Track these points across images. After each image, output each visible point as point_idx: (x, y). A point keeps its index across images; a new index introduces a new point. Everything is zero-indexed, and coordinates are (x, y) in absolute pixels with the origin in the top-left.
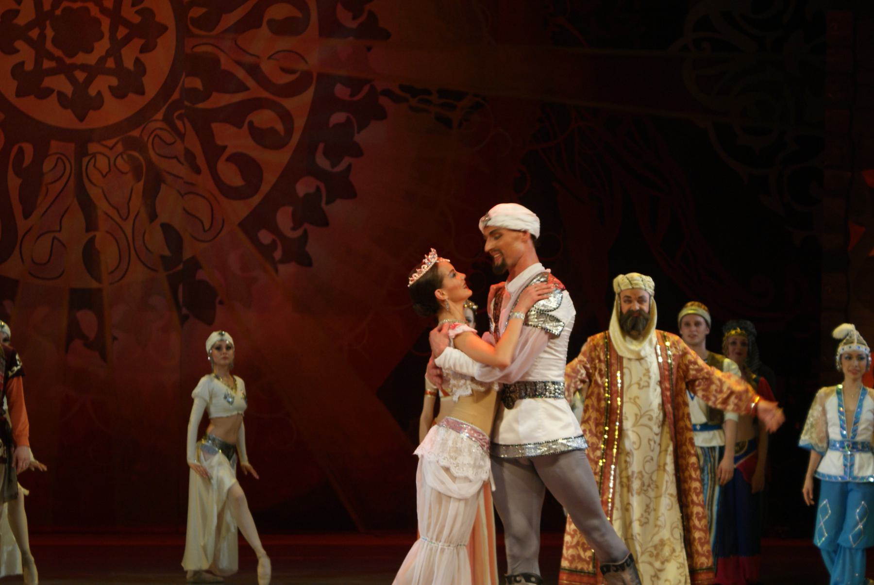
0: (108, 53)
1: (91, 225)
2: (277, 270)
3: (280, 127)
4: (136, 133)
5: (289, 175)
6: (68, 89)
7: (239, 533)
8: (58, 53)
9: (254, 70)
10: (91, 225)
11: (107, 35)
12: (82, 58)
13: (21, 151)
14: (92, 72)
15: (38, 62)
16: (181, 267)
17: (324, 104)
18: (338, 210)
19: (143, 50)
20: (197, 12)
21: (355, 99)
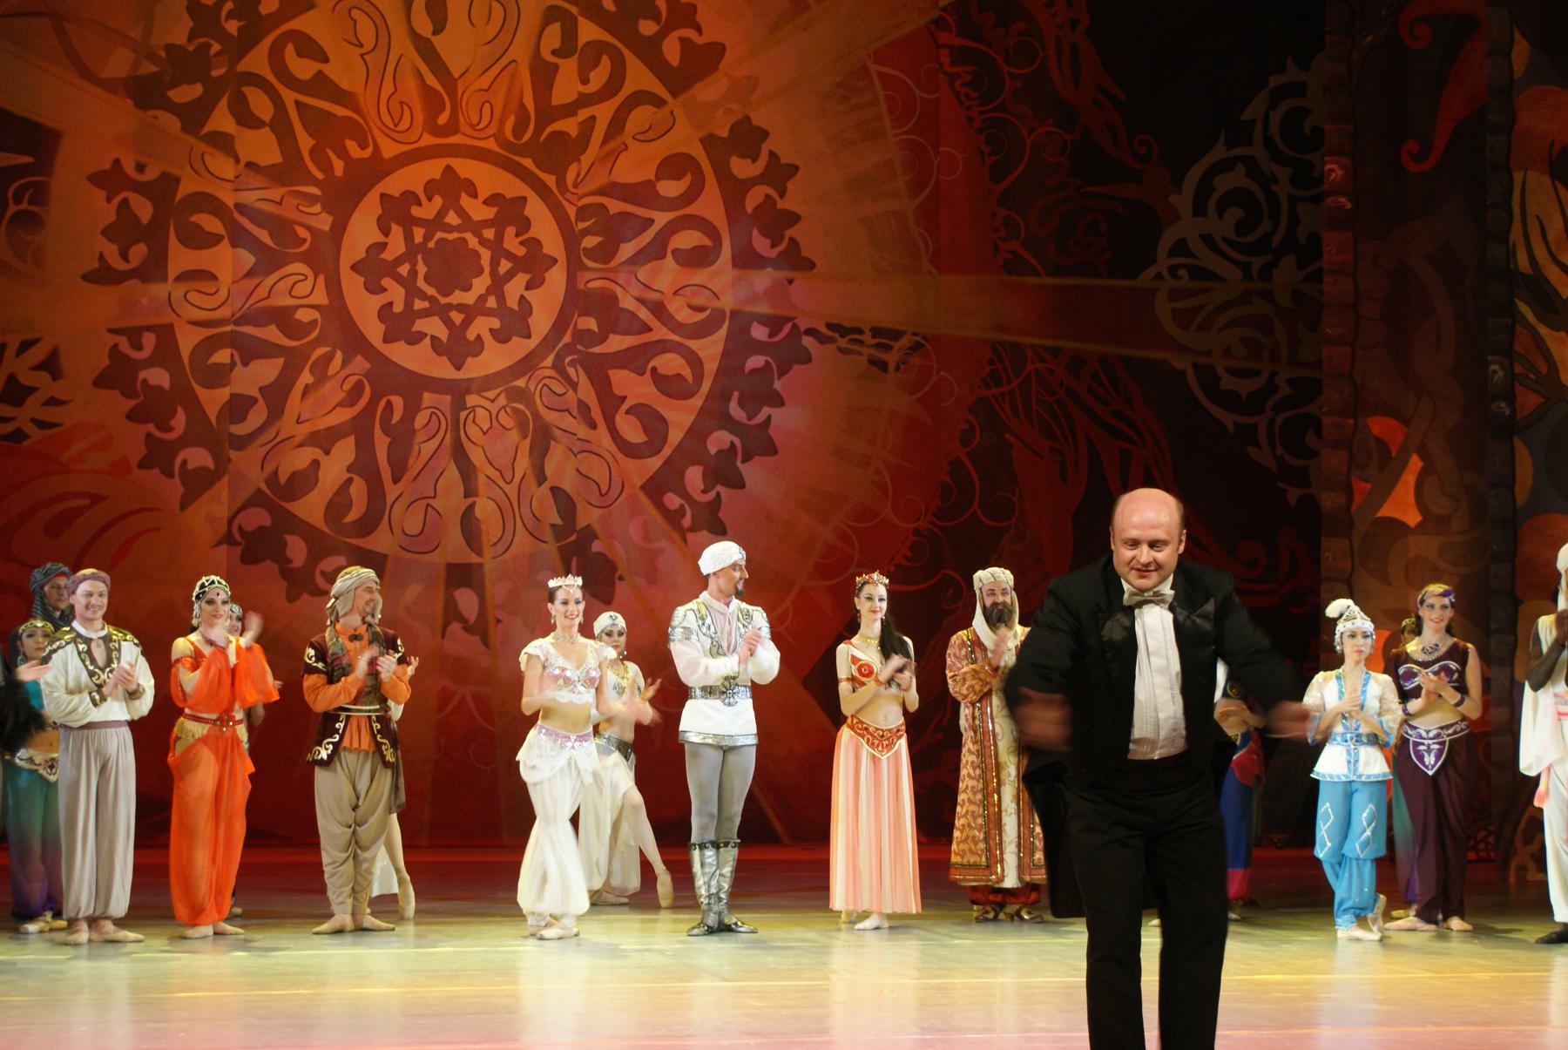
0: (489, 291)
1: (470, 492)
2: (685, 541)
3: (687, 372)
4: (521, 383)
5: (697, 434)
6: (443, 333)
7: (641, 853)
8: (431, 291)
9: (658, 310)
10: (470, 492)
11: (487, 269)
12: (458, 297)
13: (389, 404)
14: (470, 313)
15: (408, 303)
16: (574, 537)
17: (739, 344)
18: (752, 472)
19: (528, 288)
20: (590, 242)
21: (776, 339)
